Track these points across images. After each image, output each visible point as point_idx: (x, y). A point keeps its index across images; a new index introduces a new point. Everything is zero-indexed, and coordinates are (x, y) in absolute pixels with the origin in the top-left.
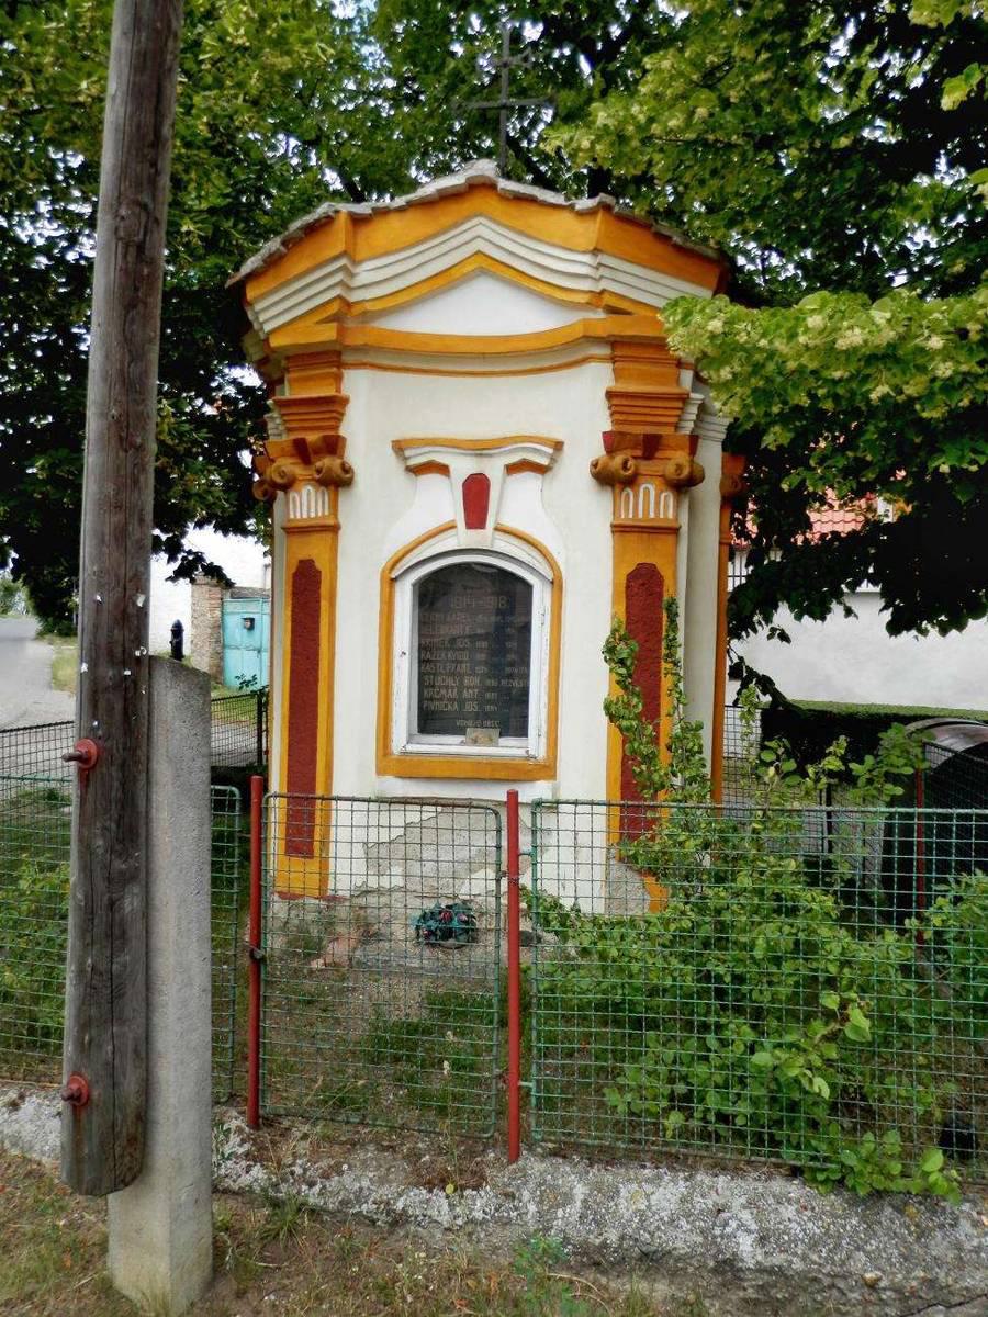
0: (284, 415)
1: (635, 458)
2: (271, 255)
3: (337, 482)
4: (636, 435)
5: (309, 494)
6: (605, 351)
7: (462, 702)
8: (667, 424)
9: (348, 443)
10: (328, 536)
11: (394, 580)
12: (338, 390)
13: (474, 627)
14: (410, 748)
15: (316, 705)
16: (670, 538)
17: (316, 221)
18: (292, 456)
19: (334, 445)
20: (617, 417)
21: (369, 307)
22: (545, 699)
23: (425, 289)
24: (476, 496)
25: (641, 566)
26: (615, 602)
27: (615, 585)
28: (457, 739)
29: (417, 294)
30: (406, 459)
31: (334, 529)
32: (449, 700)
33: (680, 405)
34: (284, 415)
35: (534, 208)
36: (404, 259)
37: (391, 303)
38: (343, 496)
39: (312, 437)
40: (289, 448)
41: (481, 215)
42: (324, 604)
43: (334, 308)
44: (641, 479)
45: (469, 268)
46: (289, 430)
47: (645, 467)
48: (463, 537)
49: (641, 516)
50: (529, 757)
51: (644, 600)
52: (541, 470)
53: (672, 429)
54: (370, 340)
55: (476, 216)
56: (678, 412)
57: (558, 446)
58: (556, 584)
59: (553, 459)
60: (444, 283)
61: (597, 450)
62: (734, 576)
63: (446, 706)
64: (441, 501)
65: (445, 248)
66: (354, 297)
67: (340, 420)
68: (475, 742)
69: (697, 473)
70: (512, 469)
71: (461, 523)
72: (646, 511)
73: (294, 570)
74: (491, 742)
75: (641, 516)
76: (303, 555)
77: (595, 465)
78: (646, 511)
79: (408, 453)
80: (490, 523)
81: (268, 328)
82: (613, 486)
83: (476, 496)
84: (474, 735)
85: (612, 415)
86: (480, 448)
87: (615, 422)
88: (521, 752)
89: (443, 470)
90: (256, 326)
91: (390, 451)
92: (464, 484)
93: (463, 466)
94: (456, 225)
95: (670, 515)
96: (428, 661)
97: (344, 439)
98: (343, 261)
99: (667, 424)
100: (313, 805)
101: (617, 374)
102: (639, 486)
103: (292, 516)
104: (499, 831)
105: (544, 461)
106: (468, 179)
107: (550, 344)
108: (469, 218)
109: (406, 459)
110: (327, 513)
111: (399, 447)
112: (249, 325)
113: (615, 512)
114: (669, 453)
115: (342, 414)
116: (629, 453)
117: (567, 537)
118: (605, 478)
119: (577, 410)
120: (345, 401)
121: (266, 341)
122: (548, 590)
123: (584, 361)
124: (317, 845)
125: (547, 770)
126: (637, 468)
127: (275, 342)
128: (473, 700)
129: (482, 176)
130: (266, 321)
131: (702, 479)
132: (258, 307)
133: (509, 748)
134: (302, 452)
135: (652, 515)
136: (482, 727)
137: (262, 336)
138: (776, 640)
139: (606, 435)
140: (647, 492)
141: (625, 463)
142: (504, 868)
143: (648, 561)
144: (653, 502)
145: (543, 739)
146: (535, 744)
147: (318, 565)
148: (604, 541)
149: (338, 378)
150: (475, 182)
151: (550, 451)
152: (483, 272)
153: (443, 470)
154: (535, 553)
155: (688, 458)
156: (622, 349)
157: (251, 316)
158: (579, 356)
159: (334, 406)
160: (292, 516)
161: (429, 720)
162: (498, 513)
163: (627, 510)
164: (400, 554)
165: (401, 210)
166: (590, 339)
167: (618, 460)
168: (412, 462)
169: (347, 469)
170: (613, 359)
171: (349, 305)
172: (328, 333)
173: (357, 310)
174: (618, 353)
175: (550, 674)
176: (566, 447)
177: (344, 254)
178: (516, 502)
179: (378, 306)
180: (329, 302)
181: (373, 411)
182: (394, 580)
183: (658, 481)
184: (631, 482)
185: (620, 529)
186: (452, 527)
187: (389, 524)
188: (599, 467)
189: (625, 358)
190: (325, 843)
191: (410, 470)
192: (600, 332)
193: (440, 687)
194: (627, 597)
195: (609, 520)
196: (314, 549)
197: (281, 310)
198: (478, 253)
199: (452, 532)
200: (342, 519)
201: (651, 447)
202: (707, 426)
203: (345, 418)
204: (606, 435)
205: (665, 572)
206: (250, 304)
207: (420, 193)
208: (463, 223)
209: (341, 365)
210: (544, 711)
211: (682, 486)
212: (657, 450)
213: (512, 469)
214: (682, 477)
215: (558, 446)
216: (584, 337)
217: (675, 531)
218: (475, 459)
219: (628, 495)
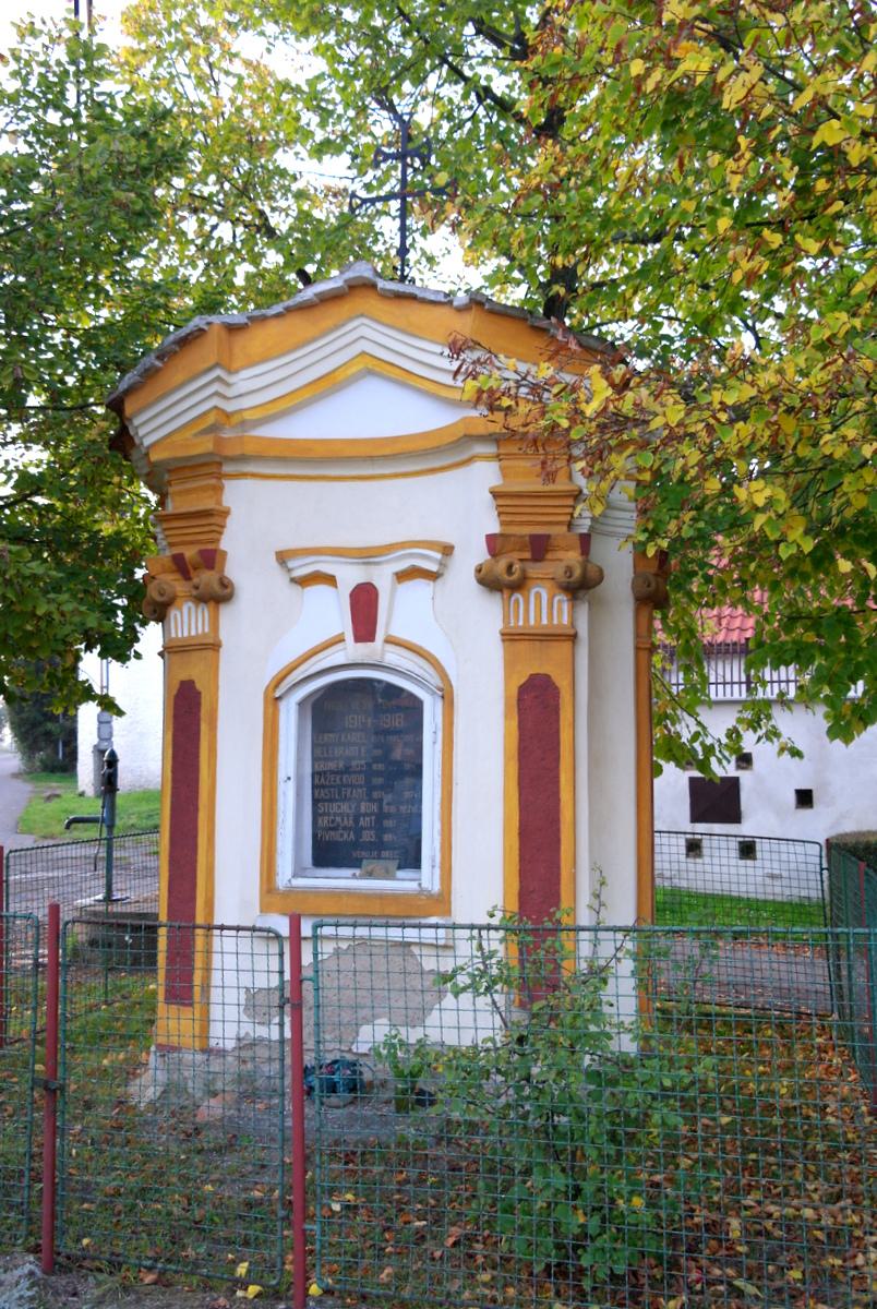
0: (165, 530)
1: (521, 560)
2: (146, 370)
3: (219, 596)
4: (522, 537)
5: (189, 609)
6: (491, 449)
7: (358, 831)
8: (558, 523)
9: (229, 556)
10: (210, 653)
11: (278, 699)
12: (219, 502)
13: (364, 758)
14: (300, 882)
15: (196, 837)
16: (567, 646)
17: (189, 334)
18: (173, 572)
19: (212, 558)
20: (504, 518)
21: (247, 416)
22: (438, 826)
23: (307, 395)
24: (364, 605)
25: (533, 677)
26: (507, 716)
27: (507, 699)
28: (348, 872)
29: (290, 405)
30: (289, 570)
31: (215, 646)
32: (345, 828)
33: (570, 502)
34: (165, 530)
35: (415, 306)
36: (278, 368)
37: (282, 406)
38: (226, 612)
39: (190, 553)
40: (168, 563)
41: (362, 315)
42: (204, 727)
43: (211, 419)
44: (529, 583)
45: (354, 370)
46: (171, 545)
47: (534, 570)
48: (351, 651)
49: (532, 622)
50: (422, 891)
51: (537, 712)
52: (433, 576)
53: (565, 528)
54: (249, 449)
55: (358, 317)
56: (570, 510)
57: (447, 550)
58: (447, 696)
59: (442, 564)
60: (327, 386)
61: (480, 554)
62: (772, 682)
63: (342, 835)
64: (328, 613)
65: (328, 350)
66: (230, 407)
67: (221, 533)
68: (370, 875)
69: (592, 574)
70: (402, 576)
71: (349, 636)
72: (527, 619)
73: (175, 692)
74: (388, 876)
75: (532, 622)
76: (184, 676)
77: (479, 570)
78: (527, 619)
79: (291, 564)
80: (380, 635)
81: (147, 442)
82: (501, 591)
83: (364, 605)
84: (369, 868)
85: (500, 514)
86: (367, 555)
87: (503, 523)
88: (414, 885)
89: (330, 580)
90: (137, 441)
91: (273, 558)
92: (351, 595)
93: (350, 575)
94: (337, 327)
95: (565, 620)
96: (323, 786)
97: (224, 554)
98: (218, 372)
99: (558, 523)
100: (155, 932)
101: (504, 472)
102: (529, 591)
103: (173, 635)
104: (281, 955)
105: (434, 568)
106: (345, 281)
107: (436, 444)
108: (351, 319)
109: (289, 570)
110: (206, 630)
111: (283, 558)
112: (131, 438)
113: (506, 618)
114: (560, 554)
115: (223, 527)
116: (516, 555)
117: (457, 648)
118: (489, 581)
119: (463, 507)
120: (225, 513)
121: (147, 454)
122: (439, 704)
123: (470, 460)
124: (197, 990)
125: (442, 901)
126: (524, 571)
127: (154, 457)
128: (370, 828)
129: (361, 277)
130: (144, 436)
131: (601, 578)
132: (136, 422)
133: (403, 883)
134: (181, 567)
135: (545, 622)
136: (379, 858)
137: (144, 451)
138: (786, 756)
139: (491, 539)
140: (538, 596)
141: (510, 567)
142: (287, 994)
143: (542, 671)
144: (544, 606)
145: (437, 871)
146: (428, 877)
147: (198, 686)
148: (493, 652)
149: (219, 489)
150: (353, 283)
151: (438, 556)
152: (370, 372)
153: (330, 580)
154: (422, 662)
155: (580, 558)
156: (506, 442)
157: (132, 433)
158: (465, 456)
159: (213, 518)
160: (173, 635)
161: (326, 854)
162: (388, 625)
163: (517, 619)
164: (284, 672)
165: (278, 316)
166: (470, 438)
167: (502, 564)
168: (298, 573)
169: (225, 584)
170: (498, 457)
171: (228, 415)
172: (205, 445)
173: (235, 419)
174: (502, 451)
175: (442, 799)
176: (456, 551)
177: (217, 365)
178: (408, 613)
179: (257, 415)
180: (205, 414)
181: (257, 519)
182: (278, 699)
183: (549, 584)
184: (519, 586)
185: (510, 637)
186: (339, 640)
187: (275, 633)
188: (483, 571)
189: (509, 456)
190: (206, 988)
191: (293, 580)
192: (481, 429)
193: (335, 815)
194: (519, 710)
195: (499, 625)
196: (194, 670)
197: (158, 425)
198: (363, 353)
199: (340, 646)
200: (223, 636)
201: (539, 548)
202: (611, 522)
203: (227, 532)
204: (491, 539)
205: (563, 683)
206: (130, 420)
207: (299, 299)
208: (343, 325)
209: (220, 476)
210: (438, 839)
211: (580, 587)
212: (547, 551)
213: (402, 576)
214: (572, 580)
215: (447, 550)
216: (465, 436)
217: (573, 638)
218: (363, 567)
219: (517, 601)
